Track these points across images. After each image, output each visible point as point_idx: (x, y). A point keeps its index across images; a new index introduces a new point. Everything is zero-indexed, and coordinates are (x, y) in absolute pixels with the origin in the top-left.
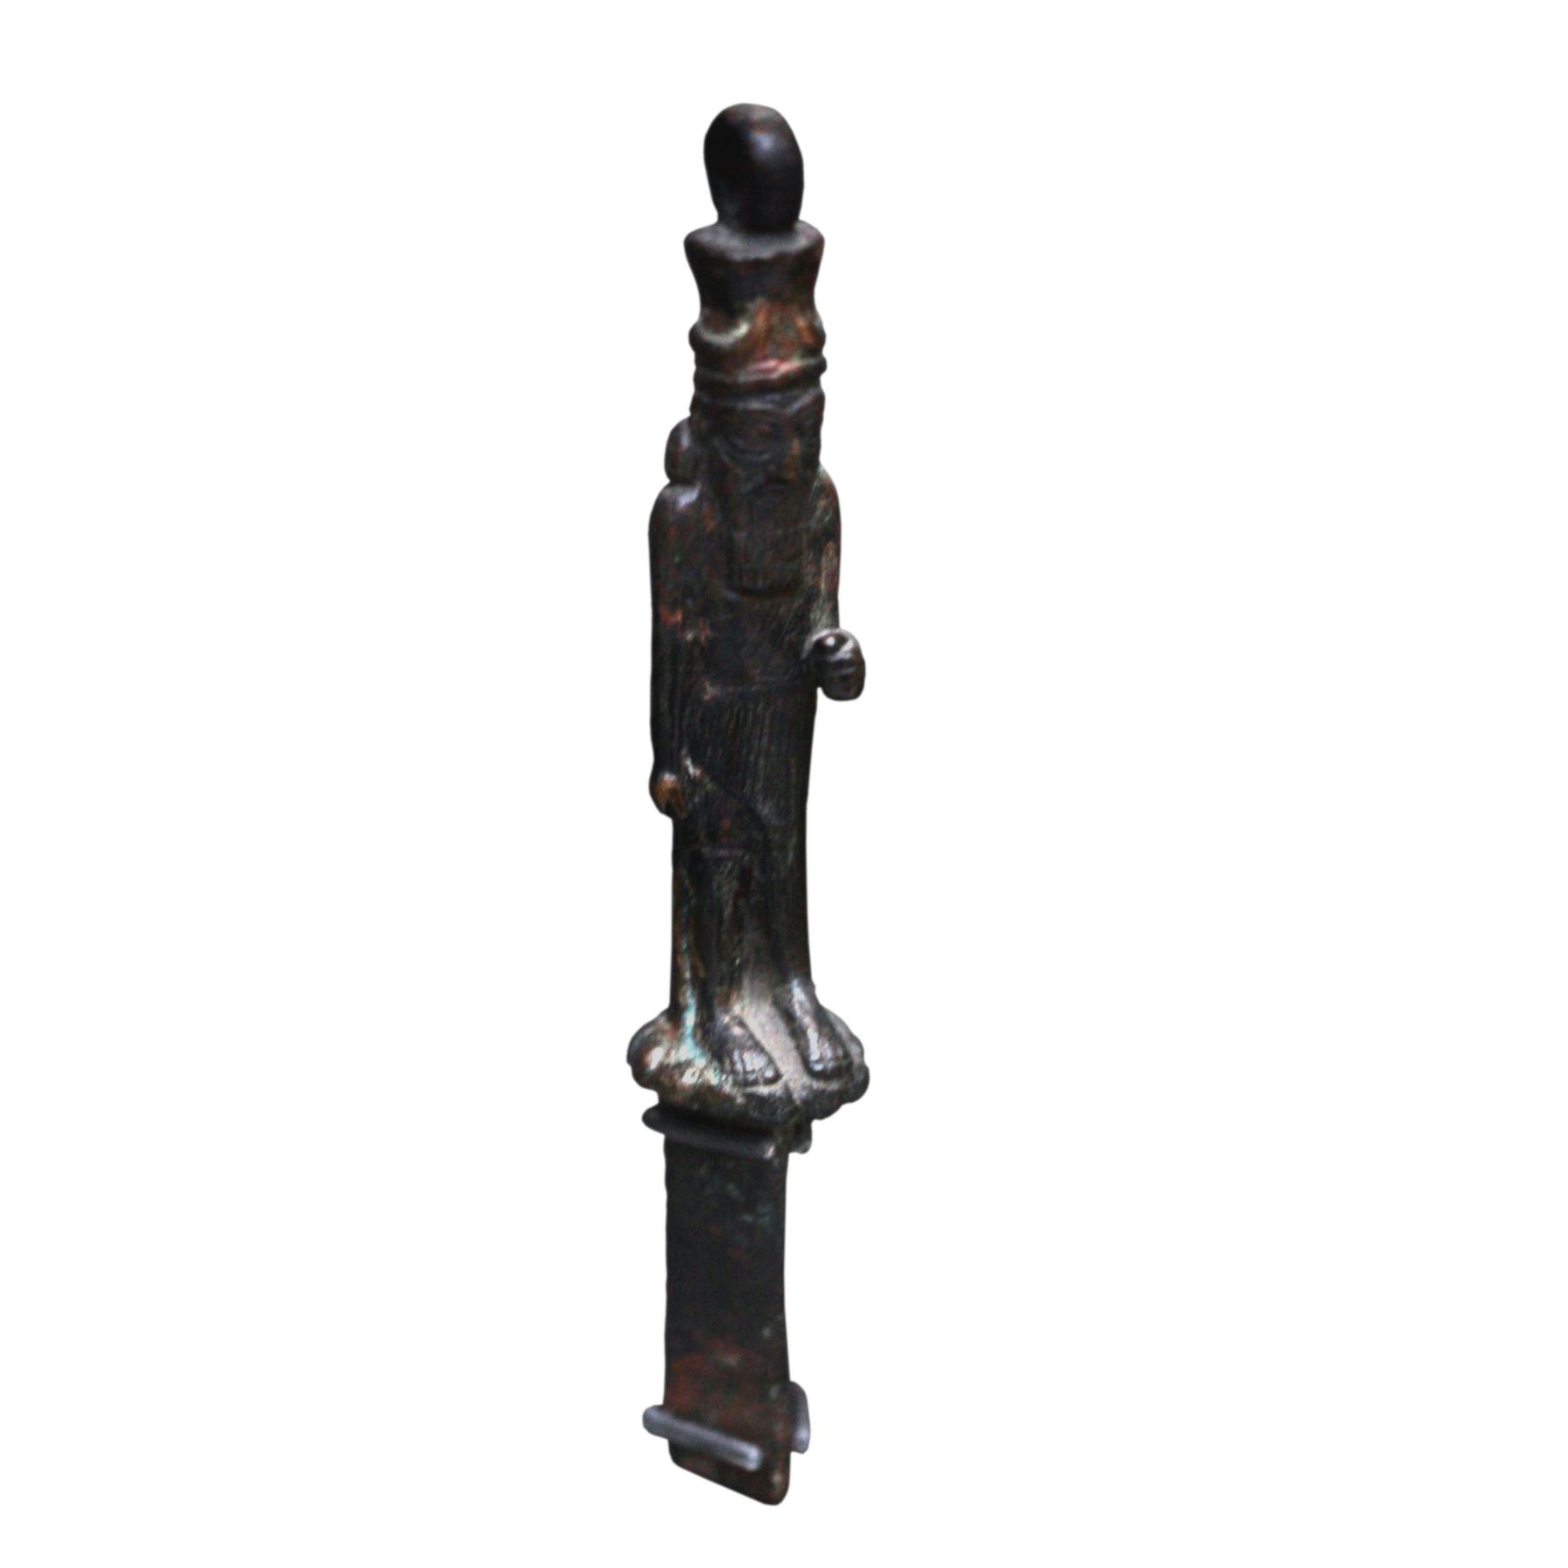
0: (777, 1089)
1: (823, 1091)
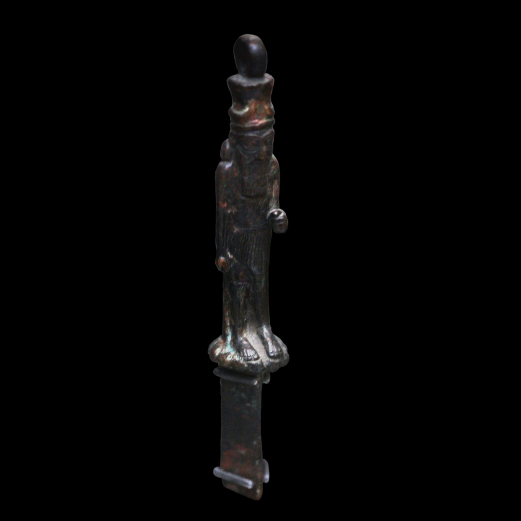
0: (258, 362)
1: (274, 363)
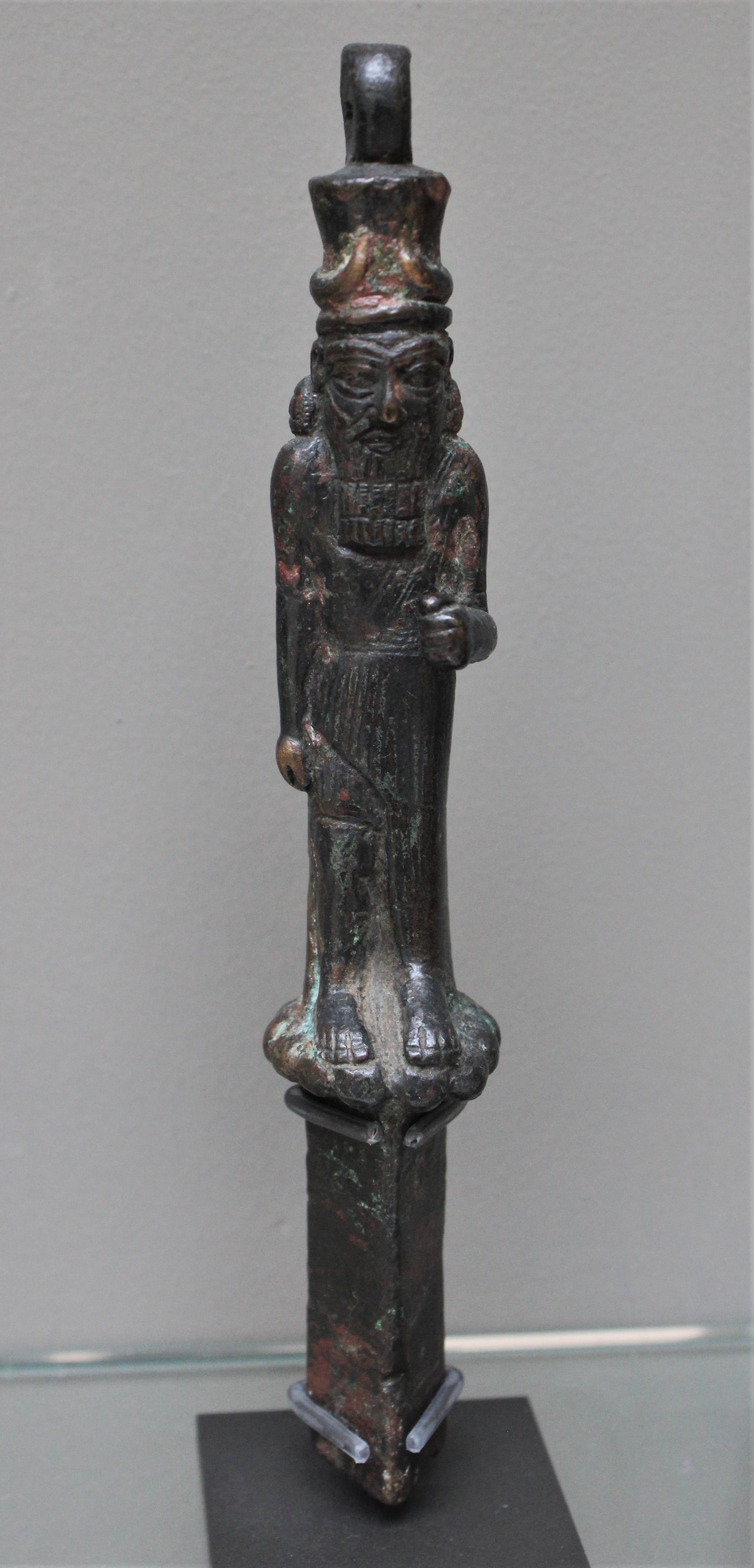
0: (368, 1071)
1: (416, 1079)
